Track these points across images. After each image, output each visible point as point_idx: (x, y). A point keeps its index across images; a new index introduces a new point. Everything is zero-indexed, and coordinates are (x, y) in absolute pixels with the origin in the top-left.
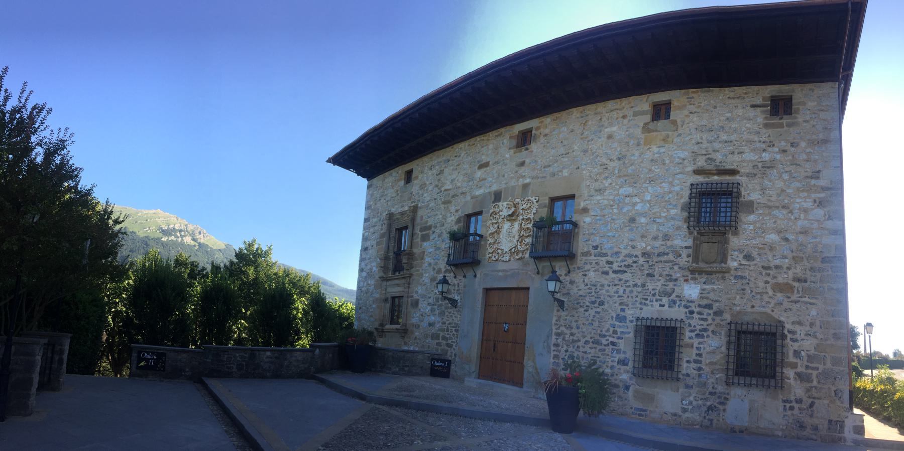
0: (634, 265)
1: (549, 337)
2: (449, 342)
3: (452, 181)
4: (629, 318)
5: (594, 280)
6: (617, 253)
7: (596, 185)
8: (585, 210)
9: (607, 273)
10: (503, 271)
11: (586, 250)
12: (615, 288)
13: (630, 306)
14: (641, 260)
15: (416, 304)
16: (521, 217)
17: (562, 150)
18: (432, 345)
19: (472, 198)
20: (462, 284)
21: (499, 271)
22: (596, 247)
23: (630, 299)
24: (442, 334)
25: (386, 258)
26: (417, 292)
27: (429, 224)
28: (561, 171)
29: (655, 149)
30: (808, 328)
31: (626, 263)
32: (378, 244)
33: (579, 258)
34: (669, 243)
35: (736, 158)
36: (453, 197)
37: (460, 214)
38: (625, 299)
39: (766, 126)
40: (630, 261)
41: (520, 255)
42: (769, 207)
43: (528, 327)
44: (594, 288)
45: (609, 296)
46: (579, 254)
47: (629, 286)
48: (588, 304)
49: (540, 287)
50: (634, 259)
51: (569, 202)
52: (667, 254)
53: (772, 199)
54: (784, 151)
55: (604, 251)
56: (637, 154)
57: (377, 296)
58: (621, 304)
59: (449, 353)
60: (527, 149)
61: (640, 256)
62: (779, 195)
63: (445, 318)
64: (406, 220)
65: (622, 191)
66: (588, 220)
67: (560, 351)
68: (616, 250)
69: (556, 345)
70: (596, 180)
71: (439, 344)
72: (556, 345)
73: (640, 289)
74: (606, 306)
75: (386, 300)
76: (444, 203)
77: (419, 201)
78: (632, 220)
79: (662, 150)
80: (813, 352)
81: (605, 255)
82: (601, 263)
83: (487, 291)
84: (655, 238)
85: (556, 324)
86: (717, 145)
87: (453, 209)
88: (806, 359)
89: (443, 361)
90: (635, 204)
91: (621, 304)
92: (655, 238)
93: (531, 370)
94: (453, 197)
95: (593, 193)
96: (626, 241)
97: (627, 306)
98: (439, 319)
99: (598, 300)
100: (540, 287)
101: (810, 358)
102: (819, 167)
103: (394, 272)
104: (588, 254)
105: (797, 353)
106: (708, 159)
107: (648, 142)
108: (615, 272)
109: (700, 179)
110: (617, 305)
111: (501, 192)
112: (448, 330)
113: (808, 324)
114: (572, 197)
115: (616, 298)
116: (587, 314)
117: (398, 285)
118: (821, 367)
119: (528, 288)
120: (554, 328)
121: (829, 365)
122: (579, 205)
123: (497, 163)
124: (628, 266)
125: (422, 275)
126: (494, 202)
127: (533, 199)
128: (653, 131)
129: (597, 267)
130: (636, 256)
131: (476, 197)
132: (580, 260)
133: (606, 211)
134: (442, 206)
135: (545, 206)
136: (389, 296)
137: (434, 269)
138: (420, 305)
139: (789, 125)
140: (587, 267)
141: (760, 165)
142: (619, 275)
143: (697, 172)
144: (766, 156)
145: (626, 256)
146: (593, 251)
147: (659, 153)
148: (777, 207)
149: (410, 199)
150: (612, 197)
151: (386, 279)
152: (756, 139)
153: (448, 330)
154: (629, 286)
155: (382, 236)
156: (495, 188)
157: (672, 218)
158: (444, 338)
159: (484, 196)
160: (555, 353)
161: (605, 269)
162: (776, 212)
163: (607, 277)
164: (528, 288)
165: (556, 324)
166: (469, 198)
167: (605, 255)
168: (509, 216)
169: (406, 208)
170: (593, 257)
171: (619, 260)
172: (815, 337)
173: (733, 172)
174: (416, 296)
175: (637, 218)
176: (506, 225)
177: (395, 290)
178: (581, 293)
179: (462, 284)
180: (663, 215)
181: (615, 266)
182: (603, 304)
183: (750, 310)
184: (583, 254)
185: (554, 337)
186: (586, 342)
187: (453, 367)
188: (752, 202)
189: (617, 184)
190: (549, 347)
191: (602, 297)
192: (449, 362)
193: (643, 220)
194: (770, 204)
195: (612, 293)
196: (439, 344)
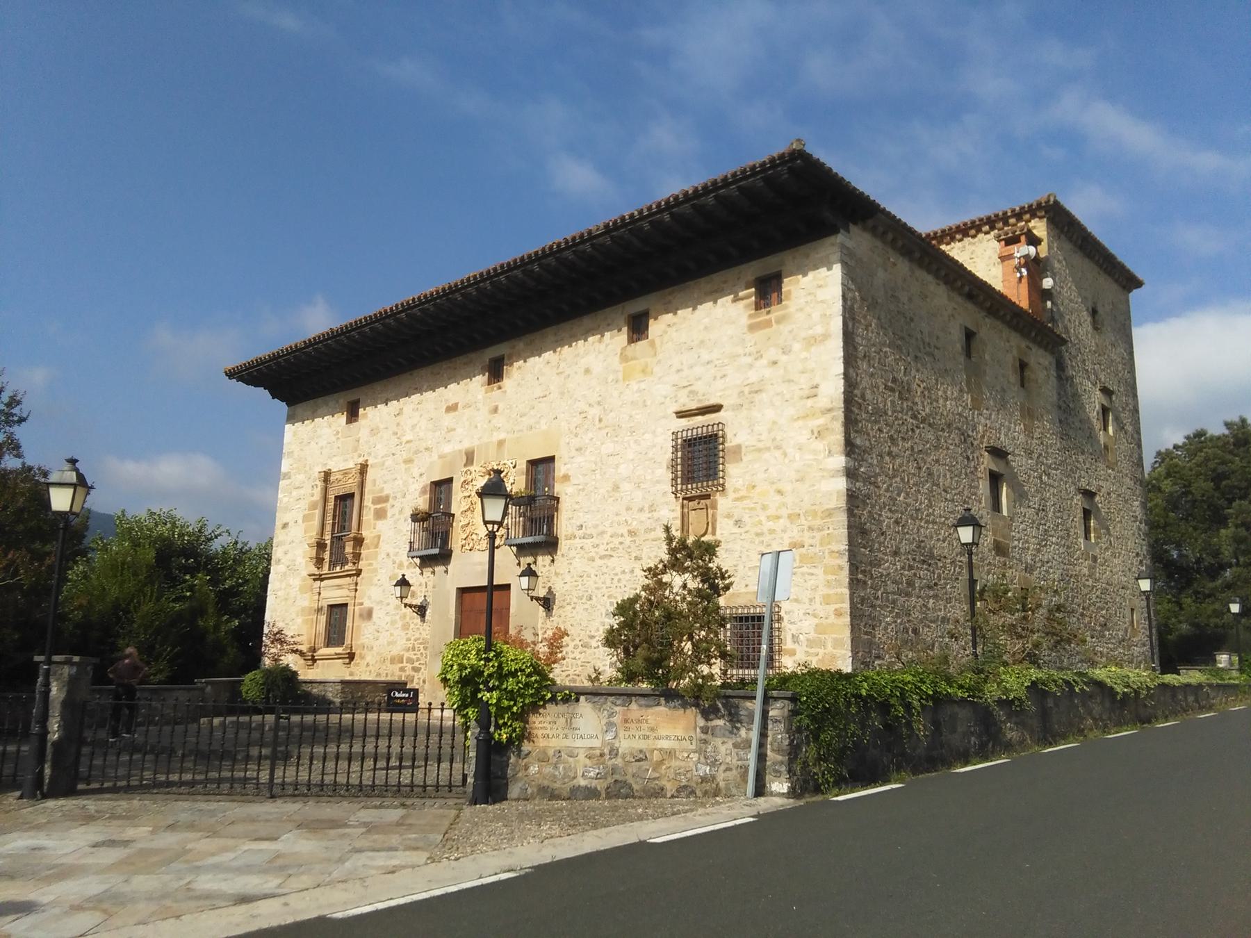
2: (416, 664)
3: (414, 426)
6: (603, 533)
7: (576, 442)
8: (566, 478)
11: (570, 532)
14: (628, 540)
15: (368, 614)
17: (539, 392)
18: (391, 673)
19: (440, 457)
20: (430, 584)
25: (321, 546)
26: (370, 598)
27: (385, 493)
28: (538, 423)
29: (634, 386)
30: (807, 606)
32: (306, 518)
34: (656, 515)
35: (719, 384)
36: (416, 452)
39: (752, 328)
42: (759, 450)
45: (598, 589)
48: (575, 600)
50: (620, 539)
52: (654, 530)
53: (763, 438)
54: (775, 363)
55: (588, 532)
56: (616, 394)
57: (306, 604)
58: (609, 597)
60: (500, 388)
61: (626, 534)
62: (770, 431)
63: (410, 632)
64: (350, 485)
68: (601, 528)
70: (576, 435)
71: (402, 669)
73: (627, 576)
75: (319, 610)
78: (616, 488)
79: (643, 386)
80: (812, 635)
82: (586, 547)
83: (462, 591)
84: (641, 510)
86: (698, 370)
87: (416, 472)
88: (805, 643)
89: (409, 691)
90: (617, 466)
92: (641, 510)
94: (416, 452)
95: (574, 453)
98: (403, 634)
101: (811, 643)
102: (816, 381)
103: (333, 564)
105: (795, 639)
106: (691, 392)
107: (627, 377)
108: (601, 558)
109: (684, 423)
111: (473, 453)
112: (414, 649)
113: (807, 601)
115: (604, 590)
117: (339, 587)
118: (821, 651)
121: (830, 648)
123: (467, 406)
124: (613, 549)
125: (375, 570)
126: (465, 465)
128: (632, 359)
132: (563, 545)
134: (403, 466)
136: (325, 604)
138: (374, 615)
139: (778, 322)
141: (747, 390)
142: (605, 561)
143: (681, 414)
144: (753, 376)
147: (639, 391)
148: (768, 449)
149: (355, 450)
151: (320, 578)
152: (741, 351)
153: (414, 649)
155: (313, 506)
156: (466, 445)
157: (658, 482)
158: (410, 661)
162: (766, 455)
163: (594, 564)
166: (435, 457)
169: (351, 465)
170: (577, 540)
172: (815, 616)
173: (716, 408)
174: (367, 604)
177: (334, 592)
179: (430, 584)
180: (648, 477)
183: (743, 590)
186: (576, 647)
187: (421, 697)
188: (739, 447)
192: (416, 691)
194: (760, 445)
195: (600, 585)
196: (402, 669)
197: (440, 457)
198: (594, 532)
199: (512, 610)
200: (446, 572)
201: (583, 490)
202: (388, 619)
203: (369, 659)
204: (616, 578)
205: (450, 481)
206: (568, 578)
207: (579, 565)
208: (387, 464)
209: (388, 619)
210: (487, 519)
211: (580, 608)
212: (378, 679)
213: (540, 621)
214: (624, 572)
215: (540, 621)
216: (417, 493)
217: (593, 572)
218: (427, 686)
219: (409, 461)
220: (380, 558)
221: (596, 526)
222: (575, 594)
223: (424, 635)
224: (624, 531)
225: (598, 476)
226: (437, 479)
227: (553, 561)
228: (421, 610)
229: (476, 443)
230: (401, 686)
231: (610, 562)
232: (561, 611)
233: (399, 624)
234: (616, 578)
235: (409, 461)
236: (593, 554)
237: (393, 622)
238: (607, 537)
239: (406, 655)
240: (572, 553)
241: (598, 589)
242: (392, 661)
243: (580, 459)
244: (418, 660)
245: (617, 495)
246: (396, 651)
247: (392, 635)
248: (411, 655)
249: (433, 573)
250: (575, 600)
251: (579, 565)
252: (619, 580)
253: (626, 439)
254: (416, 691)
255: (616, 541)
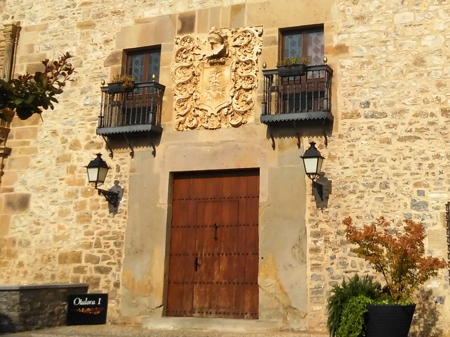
0: (432, 128)
1: (302, 239)
2: (104, 264)
4: (432, 203)
5: (368, 154)
6: (401, 112)
8: (342, 49)
9: (389, 142)
10: (209, 144)
11: (350, 108)
12: (405, 163)
13: (432, 186)
16: (235, 60)
18: (64, 275)
19: (138, 22)
21: (200, 145)
22: (367, 104)
23: (430, 177)
24: (85, 252)
26: (24, 183)
31: (418, 126)
33: (340, 122)
36: (98, 16)
37: (116, 47)
38: (422, 178)
40: (423, 122)
41: (239, 119)
43: (261, 228)
44: (370, 164)
46: (340, 115)
47: (427, 159)
48: (362, 188)
49: (280, 166)
51: (313, 36)
55: (379, 110)
58: (416, 185)
59: (102, 283)
61: (439, 115)
65: (398, 19)
66: (348, 63)
67: (322, 259)
68: (398, 106)
69: (316, 250)
72: (316, 250)
74: (392, 189)
76: (81, 26)
77: (23, 16)
78: (419, 61)
81: (384, 115)
83: (176, 176)
85: (311, 221)
87: (98, 38)
89: (94, 297)
90: (420, 38)
91: (416, 185)
93: (272, 290)
94: (98, 16)
95: (351, 22)
96: (413, 93)
97: (427, 186)
98: (80, 227)
99: (379, 181)
100: (280, 166)
104: (356, 115)
108: (400, 140)
110: (411, 186)
114: (319, 28)
115: (408, 176)
116: (362, 202)
119: (255, 172)
120: (308, 226)
122: (332, 41)
125: (34, 150)
127: (253, 30)
129: (371, 133)
130: (432, 115)
131: (146, 21)
132: (341, 125)
133: (375, 51)
134: (78, 32)
135: (273, 42)
137: (64, 141)
138: (32, 205)
140: (355, 134)
142: (408, 143)
145: (416, 115)
146: (361, 111)
150: (383, 28)
153: (98, 245)
154: (427, 159)
158: (90, 259)
159: (161, 20)
160: (314, 262)
161: (384, 136)
163: (389, 147)
164: (255, 172)
165: (311, 221)
166: (129, 22)
167: (384, 115)
168: (213, 57)
170: (362, 120)
171: (407, 121)
175: (427, 59)
176: (207, 74)
178: (348, 172)
181: (401, 131)
182: (386, 187)
184: (345, 116)
185: (310, 240)
187: (111, 304)
189: (389, 9)
190: (304, 255)
191: (385, 177)
192: (105, 297)
193: (437, 60)
196: (80, 270)
197: (138, 22)
198: (388, 110)
199: (262, 199)
200: (154, 153)
201: (369, 63)
202: (55, 208)
203: (22, 257)
204: (425, 165)
205: (157, 49)
206: (349, 162)
207: (365, 147)
208: (51, 27)
209: (55, 208)
210: (90, 180)
211: (370, 198)
212: (39, 283)
213: (308, 214)
214: (438, 156)
215: (308, 214)
216: (101, 63)
217: (388, 156)
218: (120, 291)
219: (87, 25)
220: (40, 136)
221: (391, 104)
222: (361, 180)
223: (115, 228)
224: (437, 109)
225: (391, 48)
226: (134, 45)
227: (283, 306)
228: (113, 198)
229: (196, 7)
230: (79, 291)
231: (417, 146)
232: (340, 201)
233: (74, 214)
234: (425, 165)
235: (87, 25)
236: (388, 135)
237: (63, 213)
238: (409, 117)
239: (85, 252)
240: (355, 134)
241: (398, 175)
242: (63, 259)
243: (361, 29)
244: (105, 258)
245: (422, 69)
246: (67, 247)
247: (60, 228)
248: (95, 252)
249: (132, 154)
250: (362, 188)
251: (365, 147)
252: (431, 166)
253: (432, 8)
254: (105, 297)
255: (423, 122)
